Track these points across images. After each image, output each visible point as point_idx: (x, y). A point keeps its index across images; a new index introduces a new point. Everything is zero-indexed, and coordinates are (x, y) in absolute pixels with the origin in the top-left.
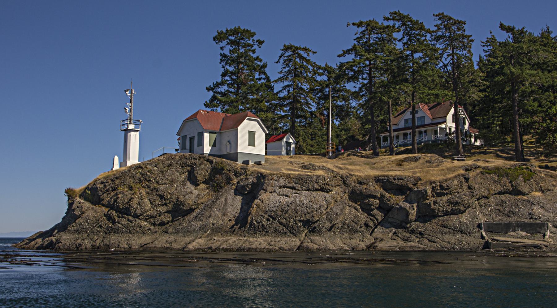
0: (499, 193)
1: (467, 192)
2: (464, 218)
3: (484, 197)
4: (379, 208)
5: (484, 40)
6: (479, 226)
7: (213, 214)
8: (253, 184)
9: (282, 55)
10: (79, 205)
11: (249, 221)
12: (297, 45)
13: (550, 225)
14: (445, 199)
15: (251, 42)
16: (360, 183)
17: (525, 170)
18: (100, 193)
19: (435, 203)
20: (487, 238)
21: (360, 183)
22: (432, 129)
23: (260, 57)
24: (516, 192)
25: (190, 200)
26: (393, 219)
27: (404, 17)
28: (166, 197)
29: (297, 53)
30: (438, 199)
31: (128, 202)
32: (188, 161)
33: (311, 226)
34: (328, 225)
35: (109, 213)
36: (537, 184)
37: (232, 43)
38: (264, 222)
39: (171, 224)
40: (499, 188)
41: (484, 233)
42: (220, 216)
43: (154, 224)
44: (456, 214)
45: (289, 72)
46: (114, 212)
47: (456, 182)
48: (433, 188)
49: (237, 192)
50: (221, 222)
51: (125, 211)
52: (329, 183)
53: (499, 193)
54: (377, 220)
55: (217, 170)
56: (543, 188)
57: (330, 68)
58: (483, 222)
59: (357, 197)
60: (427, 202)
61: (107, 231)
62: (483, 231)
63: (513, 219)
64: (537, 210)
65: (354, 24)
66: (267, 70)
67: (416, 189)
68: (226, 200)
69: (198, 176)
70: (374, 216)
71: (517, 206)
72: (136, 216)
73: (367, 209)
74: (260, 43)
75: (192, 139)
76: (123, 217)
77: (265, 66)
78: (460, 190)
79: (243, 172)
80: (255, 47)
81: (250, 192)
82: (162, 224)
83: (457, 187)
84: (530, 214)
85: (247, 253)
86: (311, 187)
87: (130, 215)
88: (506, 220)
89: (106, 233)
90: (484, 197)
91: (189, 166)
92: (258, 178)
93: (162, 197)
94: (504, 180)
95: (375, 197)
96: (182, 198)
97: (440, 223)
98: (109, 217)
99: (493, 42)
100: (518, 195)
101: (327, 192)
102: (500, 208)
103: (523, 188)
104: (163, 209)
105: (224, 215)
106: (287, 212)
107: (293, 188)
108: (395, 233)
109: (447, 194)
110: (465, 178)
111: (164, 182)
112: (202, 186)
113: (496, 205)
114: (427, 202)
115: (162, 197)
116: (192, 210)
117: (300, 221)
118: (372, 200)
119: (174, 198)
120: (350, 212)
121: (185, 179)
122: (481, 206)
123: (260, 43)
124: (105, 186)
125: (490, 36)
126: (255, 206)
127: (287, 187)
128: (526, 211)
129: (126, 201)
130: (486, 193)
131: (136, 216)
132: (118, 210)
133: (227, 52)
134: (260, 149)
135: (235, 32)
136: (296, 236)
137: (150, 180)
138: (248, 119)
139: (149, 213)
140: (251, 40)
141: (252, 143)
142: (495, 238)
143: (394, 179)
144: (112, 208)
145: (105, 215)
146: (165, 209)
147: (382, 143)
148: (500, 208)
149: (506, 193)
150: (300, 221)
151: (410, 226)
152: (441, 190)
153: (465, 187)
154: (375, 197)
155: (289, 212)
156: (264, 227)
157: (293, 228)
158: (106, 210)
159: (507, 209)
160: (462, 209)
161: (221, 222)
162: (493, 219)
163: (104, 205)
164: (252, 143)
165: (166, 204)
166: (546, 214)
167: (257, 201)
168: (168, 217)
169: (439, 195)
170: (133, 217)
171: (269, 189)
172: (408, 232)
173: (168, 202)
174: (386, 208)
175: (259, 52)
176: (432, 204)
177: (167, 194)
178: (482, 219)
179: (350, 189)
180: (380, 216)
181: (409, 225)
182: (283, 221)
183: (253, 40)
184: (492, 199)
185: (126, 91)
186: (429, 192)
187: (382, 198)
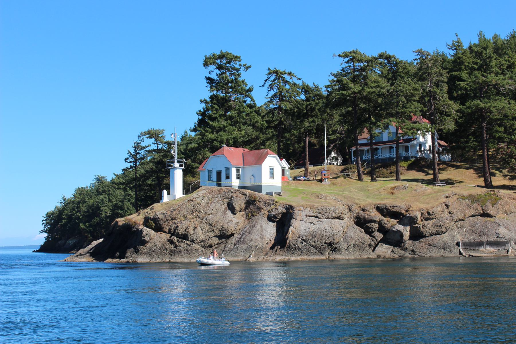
0: (473, 216)
1: (448, 216)
2: (445, 237)
3: (460, 220)
4: (379, 230)
5: (450, 43)
6: (458, 244)
7: (254, 238)
8: (283, 213)
9: (267, 80)
10: (147, 233)
11: (287, 244)
12: (282, 70)
13: (512, 242)
14: (430, 222)
15: (237, 66)
16: (363, 210)
17: (492, 196)
18: (161, 222)
19: (423, 226)
20: (464, 254)
21: (363, 210)
22: (403, 146)
23: (246, 81)
24: (485, 215)
25: (231, 228)
26: (392, 239)
27: (390, 57)
28: (213, 225)
29: (282, 77)
30: (426, 223)
31: (186, 230)
32: (226, 194)
33: (333, 247)
34: (345, 246)
35: (172, 238)
36: (503, 207)
37: (220, 67)
38: (299, 245)
39: (216, 246)
40: (472, 212)
41: (461, 250)
42: (260, 240)
43: (204, 247)
44: (439, 234)
45: (275, 96)
46: (175, 238)
47: (439, 209)
48: (422, 214)
49: (270, 219)
50: (261, 244)
51: (185, 237)
52: (344, 212)
53: (473, 216)
54: (376, 240)
55: (250, 202)
56: (507, 211)
57: (308, 86)
58: (460, 240)
59: (361, 222)
60: (417, 225)
61: (171, 253)
62: (460, 247)
63: (484, 239)
64: (502, 231)
65: (340, 56)
66: (252, 94)
67: (408, 215)
68: (261, 226)
69: (236, 207)
70: (374, 237)
71: (486, 227)
72: (193, 241)
73: (369, 232)
74: (247, 68)
75: (219, 173)
76: (182, 242)
77: (250, 90)
78: (442, 215)
79: (271, 203)
80: (242, 71)
81: (283, 221)
82: (210, 246)
83: (440, 213)
84: (497, 233)
85: (132, 266)
86: (330, 216)
87: (188, 240)
88: (478, 240)
89: (171, 255)
90: (460, 220)
91: (227, 198)
92: (287, 209)
93: (210, 224)
94: (475, 205)
95: (374, 221)
96: (225, 226)
97: (427, 242)
98: (172, 242)
99: (459, 46)
100: (488, 217)
101: (342, 219)
102: (473, 229)
103: (491, 211)
104: (212, 234)
105: (262, 239)
106: (315, 236)
107: (317, 217)
108: (392, 251)
109: (432, 219)
110: (446, 205)
111: (210, 212)
112: (239, 214)
113: (469, 226)
114: (417, 225)
115: (210, 224)
116: (232, 235)
117: (325, 243)
118: (373, 224)
119: (219, 226)
120: (357, 234)
121: (225, 209)
122: (458, 228)
123: (247, 68)
124: (165, 216)
125: (456, 39)
126: (291, 232)
127: (311, 216)
128: (493, 232)
129: (185, 229)
130: (461, 217)
131: (193, 241)
132: (178, 235)
133: (214, 76)
134: (277, 181)
135: (221, 57)
136: (323, 254)
137: (200, 211)
138: (269, 156)
139: (201, 238)
140: (238, 64)
141: (272, 175)
142: (471, 254)
143: (391, 207)
144: (172, 235)
145: (168, 241)
146: (212, 234)
147: (352, 157)
148: (473, 229)
149: (478, 216)
150: (325, 243)
151: (404, 245)
152: (428, 216)
153: (446, 213)
154: (374, 221)
155: (317, 236)
156: (299, 249)
157: (320, 249)
158: (168, 236)
159: (479, 230)
160: (444, 230)
161: (261, 244)
162: (468, 238)
163: (165, 232)
164: (272, 175)
165: (213, 231)
166: (510, 233)
167: (291, 228)
168: (216, 240)
169: (427, 219)
170: (191, 241)
171: (298, 218)
172: (402, 249)
173: (215, 228)
174: (382, 229)
175: (244, 76)
176: (421, 227)
177: (214, 223)
178: (459, 238)
179: (355, 215)
180: (379, 236)
181: (403, 244)
182: (313, 244)
183: (240, 65)
184: (467, 222)
185: (171, 135)
186: (419, 217)
187: (380, 224)
